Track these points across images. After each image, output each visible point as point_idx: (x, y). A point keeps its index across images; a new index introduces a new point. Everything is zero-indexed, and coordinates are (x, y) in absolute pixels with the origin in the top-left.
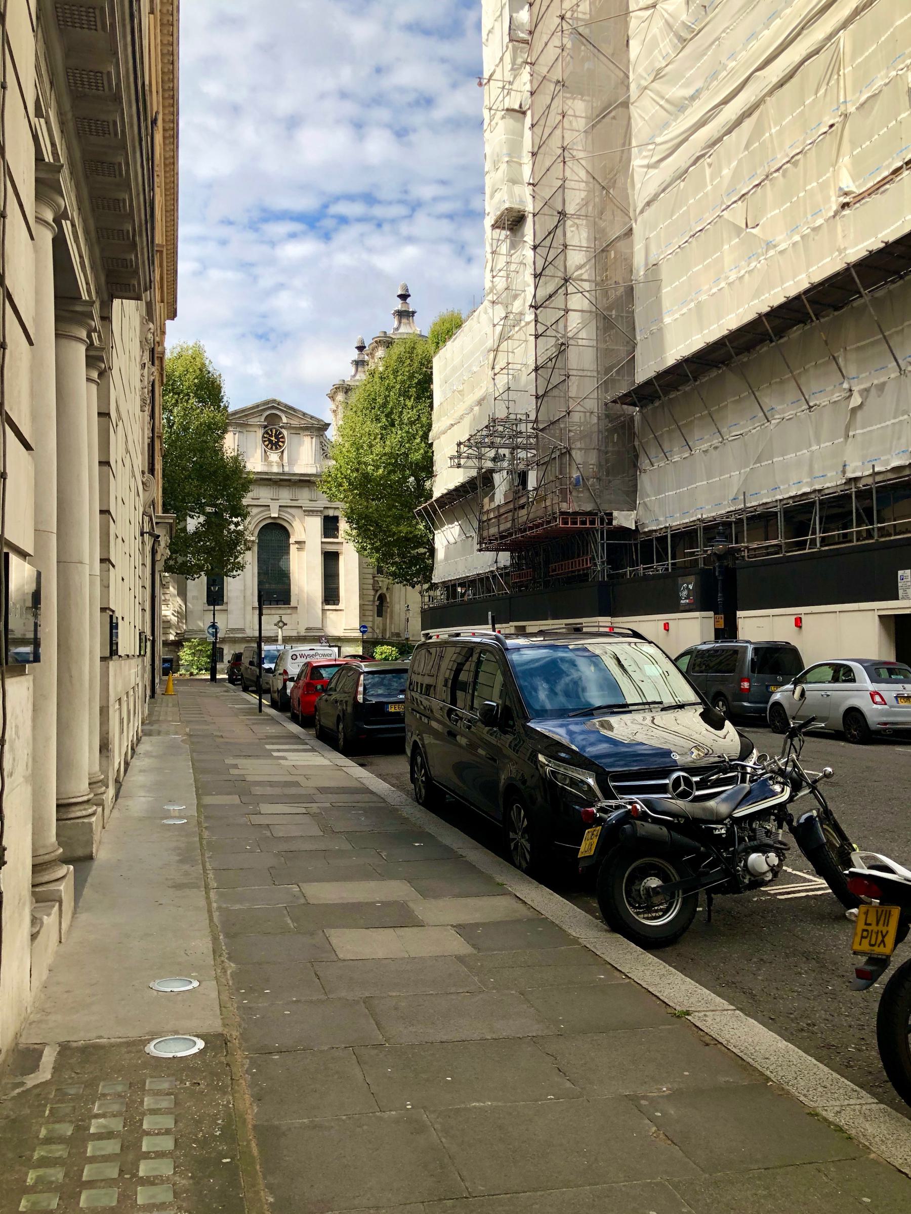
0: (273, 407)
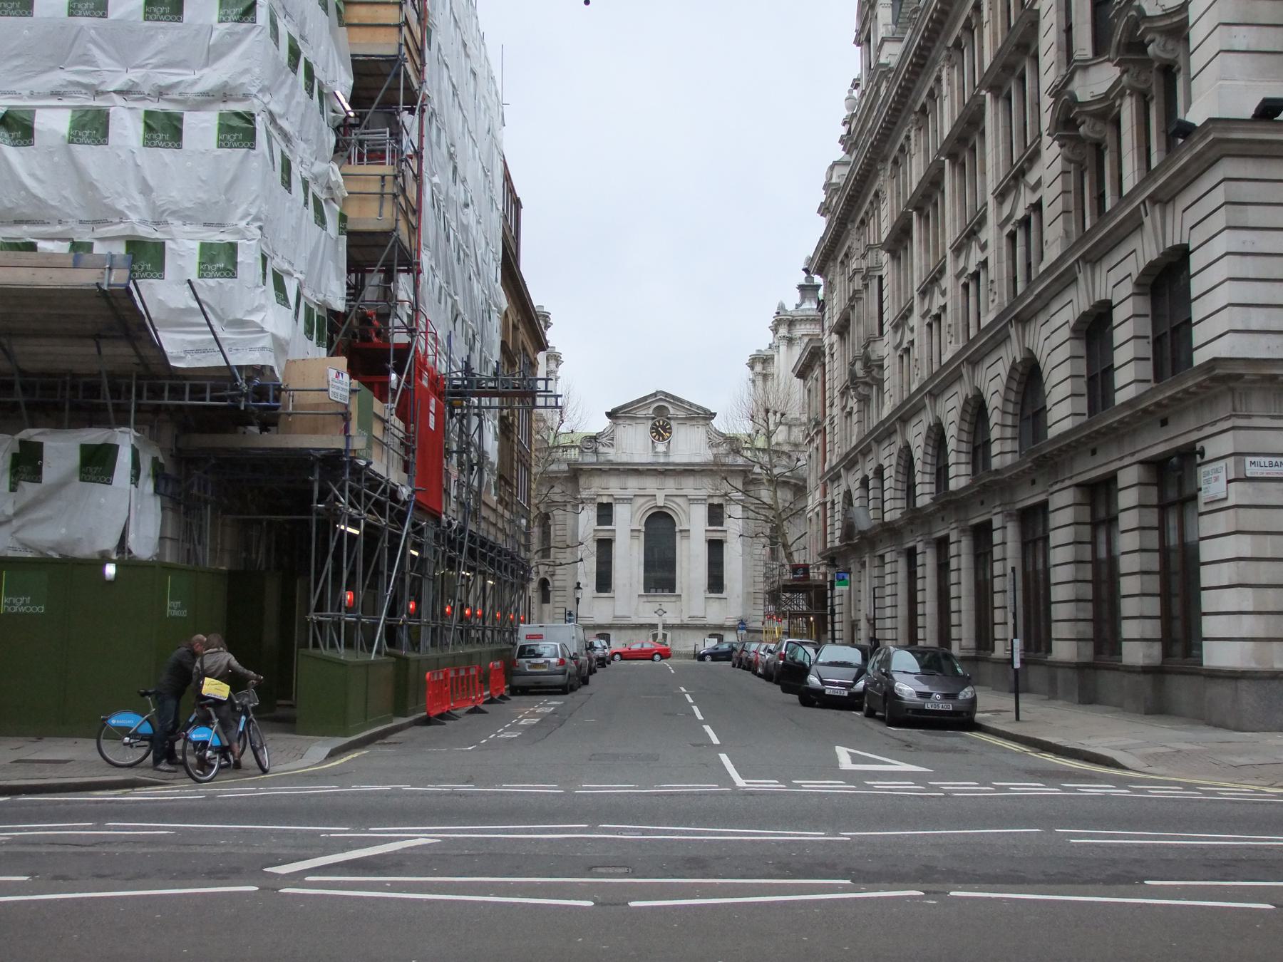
0: (661, 399)
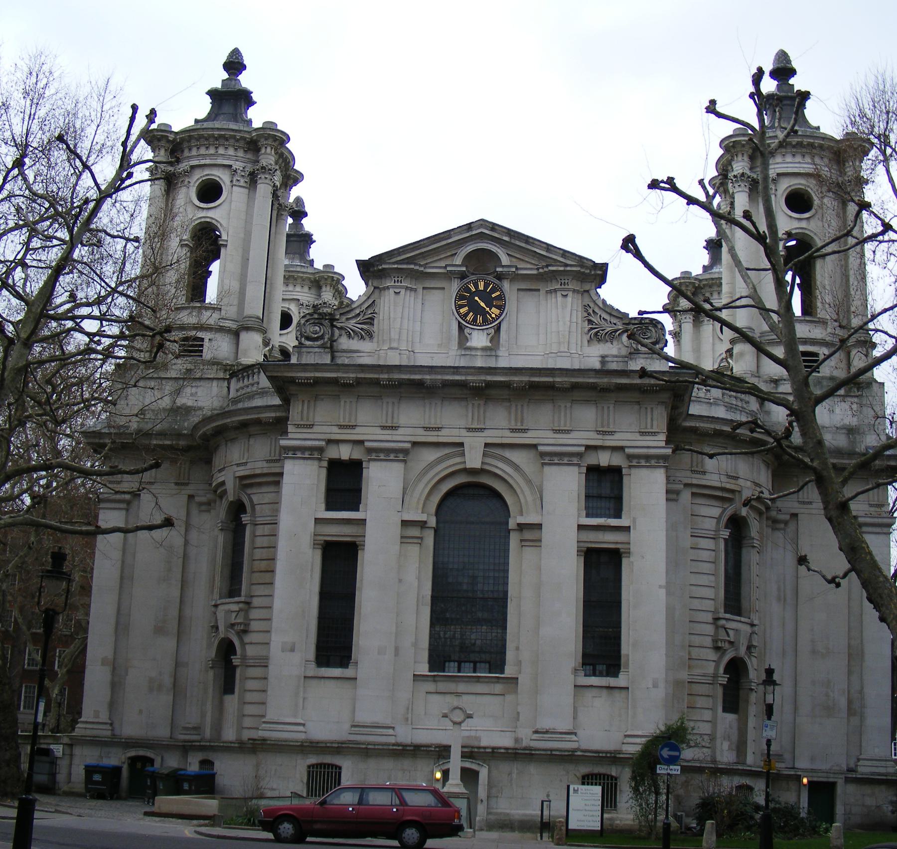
0: (481, 236)
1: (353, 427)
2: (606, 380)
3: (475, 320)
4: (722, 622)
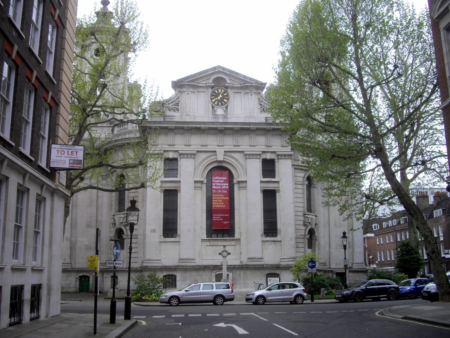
0: (219, 72)
1: (174, 145)
2: (269, 127)
3: (218, 104)
4: (307, 215)
